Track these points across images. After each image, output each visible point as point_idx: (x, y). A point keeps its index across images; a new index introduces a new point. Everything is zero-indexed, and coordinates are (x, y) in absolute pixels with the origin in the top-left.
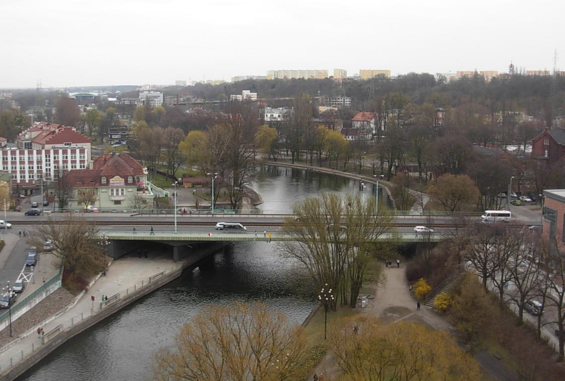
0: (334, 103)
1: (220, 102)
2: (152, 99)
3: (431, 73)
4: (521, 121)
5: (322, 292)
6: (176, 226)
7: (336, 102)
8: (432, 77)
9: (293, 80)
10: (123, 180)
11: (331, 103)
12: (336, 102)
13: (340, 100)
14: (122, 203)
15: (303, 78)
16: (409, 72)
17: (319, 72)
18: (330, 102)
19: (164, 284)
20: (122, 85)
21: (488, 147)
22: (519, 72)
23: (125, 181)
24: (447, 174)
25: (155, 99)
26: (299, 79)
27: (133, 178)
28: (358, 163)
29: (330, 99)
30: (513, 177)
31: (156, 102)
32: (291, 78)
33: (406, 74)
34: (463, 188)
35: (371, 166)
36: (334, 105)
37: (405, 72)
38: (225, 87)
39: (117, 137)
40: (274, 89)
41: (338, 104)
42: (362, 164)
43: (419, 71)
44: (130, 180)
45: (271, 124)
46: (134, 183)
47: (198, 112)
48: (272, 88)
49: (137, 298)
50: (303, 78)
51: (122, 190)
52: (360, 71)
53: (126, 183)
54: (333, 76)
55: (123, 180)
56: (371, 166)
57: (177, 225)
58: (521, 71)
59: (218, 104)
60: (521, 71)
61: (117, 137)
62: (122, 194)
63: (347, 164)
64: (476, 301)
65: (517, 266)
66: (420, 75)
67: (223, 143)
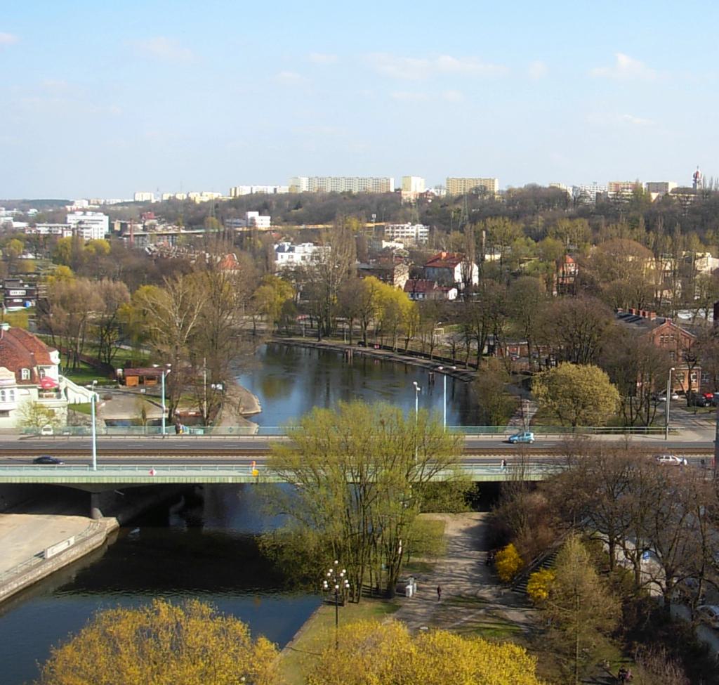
0: (400, 235)
1: (206, 233)
2: (88, 226)
3: (563, 187)
4: (704, 269)
5: (329, 574)
6: (95, 457)
7: (402, 233)
8: (565, 194)
9: (333, 194)
10: (13, 374)
11: (395, 235)
12: (402, 233)
13: (410, 230)
14: (10, 413)
15: (350, 192)
16: (527, 183)
17: (377, 182)
18: (393, 232)
19: (71, 561)
20: (40, 199)
21: (289, 429)
22: (708, 186)
23: (16, 376)
24: (564, 363)
25: (93, 226)
26: (343, 193)
27: (32, 372)
28: (428, 341)
29: (393, 228)
30: (673, 369)
31: (96, 231)
32: (329, 191)
33: (523, 186)
34: (590, 388)
35: (449, 345)
36: (398, 239)
37: (519, 183)
38: (217, 206)
39: (19, 293)
40: (300, 210)
41: (407, 237)
42: (435, 342)
43: (544, 182)
44: (25, 374)
45: (287, 274)
46: (32, 380)
47: (162, 248)
48: (296, 208)
49: (21, 588)
50: (350, 192)
51: (12, 392)
52: (448, 179)
53: (19, 379)
54: (401, 188)
55: (13, 374)
56: (449, 345)
57: (97, 454)
58: (711, 184)
59: (201, 236)
60: (711, 184)
61: (19, 293)
62: (13, 398)
63: (410, 343)
64: (581, 588)
65: (119, 633)
66: (545, 189)
67: (192, 309)
